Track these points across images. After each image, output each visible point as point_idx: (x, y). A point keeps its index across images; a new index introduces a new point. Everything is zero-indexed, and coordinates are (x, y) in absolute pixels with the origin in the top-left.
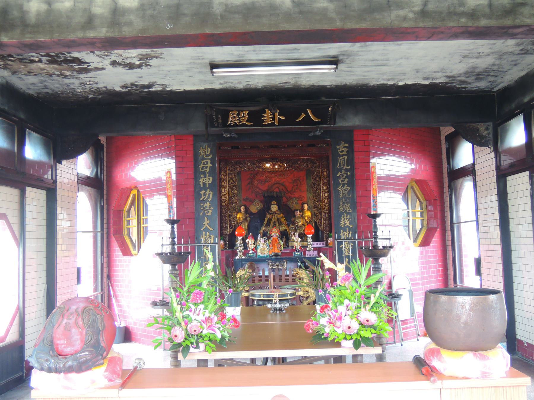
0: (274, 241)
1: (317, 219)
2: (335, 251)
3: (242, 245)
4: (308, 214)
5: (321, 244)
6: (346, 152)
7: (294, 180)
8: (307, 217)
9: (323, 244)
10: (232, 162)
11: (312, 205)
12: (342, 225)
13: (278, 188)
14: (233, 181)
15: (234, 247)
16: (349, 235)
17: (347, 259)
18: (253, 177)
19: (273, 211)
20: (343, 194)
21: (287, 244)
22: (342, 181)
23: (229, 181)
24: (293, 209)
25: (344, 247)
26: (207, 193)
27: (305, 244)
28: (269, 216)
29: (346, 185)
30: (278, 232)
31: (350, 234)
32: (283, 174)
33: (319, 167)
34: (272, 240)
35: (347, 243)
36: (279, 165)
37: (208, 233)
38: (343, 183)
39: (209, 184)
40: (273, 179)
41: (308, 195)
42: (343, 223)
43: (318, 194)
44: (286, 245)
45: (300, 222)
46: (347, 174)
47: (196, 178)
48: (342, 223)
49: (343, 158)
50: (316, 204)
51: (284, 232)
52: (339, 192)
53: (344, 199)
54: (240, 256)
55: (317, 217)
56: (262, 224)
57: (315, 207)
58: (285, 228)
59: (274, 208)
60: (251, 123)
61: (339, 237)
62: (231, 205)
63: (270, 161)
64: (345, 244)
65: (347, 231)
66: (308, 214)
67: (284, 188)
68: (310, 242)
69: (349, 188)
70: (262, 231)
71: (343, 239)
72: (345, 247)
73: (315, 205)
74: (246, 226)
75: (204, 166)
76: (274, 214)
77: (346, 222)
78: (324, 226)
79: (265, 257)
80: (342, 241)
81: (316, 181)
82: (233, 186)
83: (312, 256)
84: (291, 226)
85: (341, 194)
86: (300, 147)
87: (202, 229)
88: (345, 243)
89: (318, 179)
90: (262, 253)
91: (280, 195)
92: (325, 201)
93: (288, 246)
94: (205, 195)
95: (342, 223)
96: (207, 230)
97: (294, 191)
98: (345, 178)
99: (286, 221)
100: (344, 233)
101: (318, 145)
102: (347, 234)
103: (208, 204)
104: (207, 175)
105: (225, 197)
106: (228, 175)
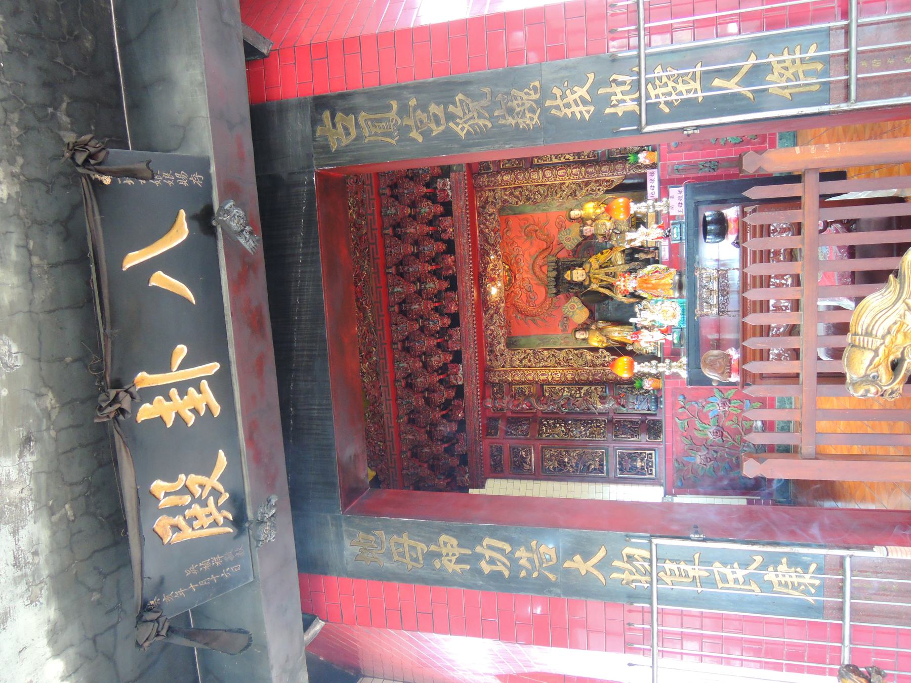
0: (645, 286)
1: (599, 190)
2: (683, 129)
4: (590, 208)
5: (653, 178)
6: (347, 115)
7: (525, 237)
8: (597, 208)
9: (652, 174)
10: (490, 360)
11: (571, 202)
12: (588, 112)
16: (624, 83)
17: (717, 82)
18: (522, 313)
20: (480, 116)
22: (438, 123)
23: (525, 366)
24: (581, 239)
25: (668, 99)
26: (488, 554)
28: (594, 286)
29: (451, 108)
30: (625, 278)
31: (621, 78)
33: (494, 190)
35: (655, 88)
37: (616, 563)
38: (443, 121)
39: (459, 545)
40: (525, 276)
41: (555, 207)
42: (581, 108)
43: (548, 191)
45: (604, 224)
46: (415, 108)
47: (443, 580)
48: (581, 112)
49: (367, 125)
50: (569, 194)
51: (627, 255)
52: (475, 131)
53: (496, 114)
54: (680, 367)
56: (612, 299)
57: (573, 194)
58: (619, 254)
59: (578, 275)
60: (216, 456)
61: (633, 118)
62: (572, 361)
63: (485, 289)
64: (657, 96)
65: (609, 90)
67: (542, 256)
69: (460, 97)
71: (640, 105)
72: (670, 94)
73: (571, 195)
74: (615, 328)
75: (407, 555)
77: (576, 96)
78: (613, 175)
80: (647, 105)
83: (683, 201)
84: (614, 243)
85: (481, 122)
86: (453, 231)
87: (603, 581)
88: (653, 93)
90: (674, 316)
91: (554, 264)
92: (560, 176)
94: (492, 561)
95: (581, 112)
96: (604, 565)
97: (547, 236)
98: (427, 111)
100: (614, 102)
101: (448, 195)
102: (618, 90)
103: (521, 553)
104: (433, 548)
105: (556, 374)
106: (514, 367)
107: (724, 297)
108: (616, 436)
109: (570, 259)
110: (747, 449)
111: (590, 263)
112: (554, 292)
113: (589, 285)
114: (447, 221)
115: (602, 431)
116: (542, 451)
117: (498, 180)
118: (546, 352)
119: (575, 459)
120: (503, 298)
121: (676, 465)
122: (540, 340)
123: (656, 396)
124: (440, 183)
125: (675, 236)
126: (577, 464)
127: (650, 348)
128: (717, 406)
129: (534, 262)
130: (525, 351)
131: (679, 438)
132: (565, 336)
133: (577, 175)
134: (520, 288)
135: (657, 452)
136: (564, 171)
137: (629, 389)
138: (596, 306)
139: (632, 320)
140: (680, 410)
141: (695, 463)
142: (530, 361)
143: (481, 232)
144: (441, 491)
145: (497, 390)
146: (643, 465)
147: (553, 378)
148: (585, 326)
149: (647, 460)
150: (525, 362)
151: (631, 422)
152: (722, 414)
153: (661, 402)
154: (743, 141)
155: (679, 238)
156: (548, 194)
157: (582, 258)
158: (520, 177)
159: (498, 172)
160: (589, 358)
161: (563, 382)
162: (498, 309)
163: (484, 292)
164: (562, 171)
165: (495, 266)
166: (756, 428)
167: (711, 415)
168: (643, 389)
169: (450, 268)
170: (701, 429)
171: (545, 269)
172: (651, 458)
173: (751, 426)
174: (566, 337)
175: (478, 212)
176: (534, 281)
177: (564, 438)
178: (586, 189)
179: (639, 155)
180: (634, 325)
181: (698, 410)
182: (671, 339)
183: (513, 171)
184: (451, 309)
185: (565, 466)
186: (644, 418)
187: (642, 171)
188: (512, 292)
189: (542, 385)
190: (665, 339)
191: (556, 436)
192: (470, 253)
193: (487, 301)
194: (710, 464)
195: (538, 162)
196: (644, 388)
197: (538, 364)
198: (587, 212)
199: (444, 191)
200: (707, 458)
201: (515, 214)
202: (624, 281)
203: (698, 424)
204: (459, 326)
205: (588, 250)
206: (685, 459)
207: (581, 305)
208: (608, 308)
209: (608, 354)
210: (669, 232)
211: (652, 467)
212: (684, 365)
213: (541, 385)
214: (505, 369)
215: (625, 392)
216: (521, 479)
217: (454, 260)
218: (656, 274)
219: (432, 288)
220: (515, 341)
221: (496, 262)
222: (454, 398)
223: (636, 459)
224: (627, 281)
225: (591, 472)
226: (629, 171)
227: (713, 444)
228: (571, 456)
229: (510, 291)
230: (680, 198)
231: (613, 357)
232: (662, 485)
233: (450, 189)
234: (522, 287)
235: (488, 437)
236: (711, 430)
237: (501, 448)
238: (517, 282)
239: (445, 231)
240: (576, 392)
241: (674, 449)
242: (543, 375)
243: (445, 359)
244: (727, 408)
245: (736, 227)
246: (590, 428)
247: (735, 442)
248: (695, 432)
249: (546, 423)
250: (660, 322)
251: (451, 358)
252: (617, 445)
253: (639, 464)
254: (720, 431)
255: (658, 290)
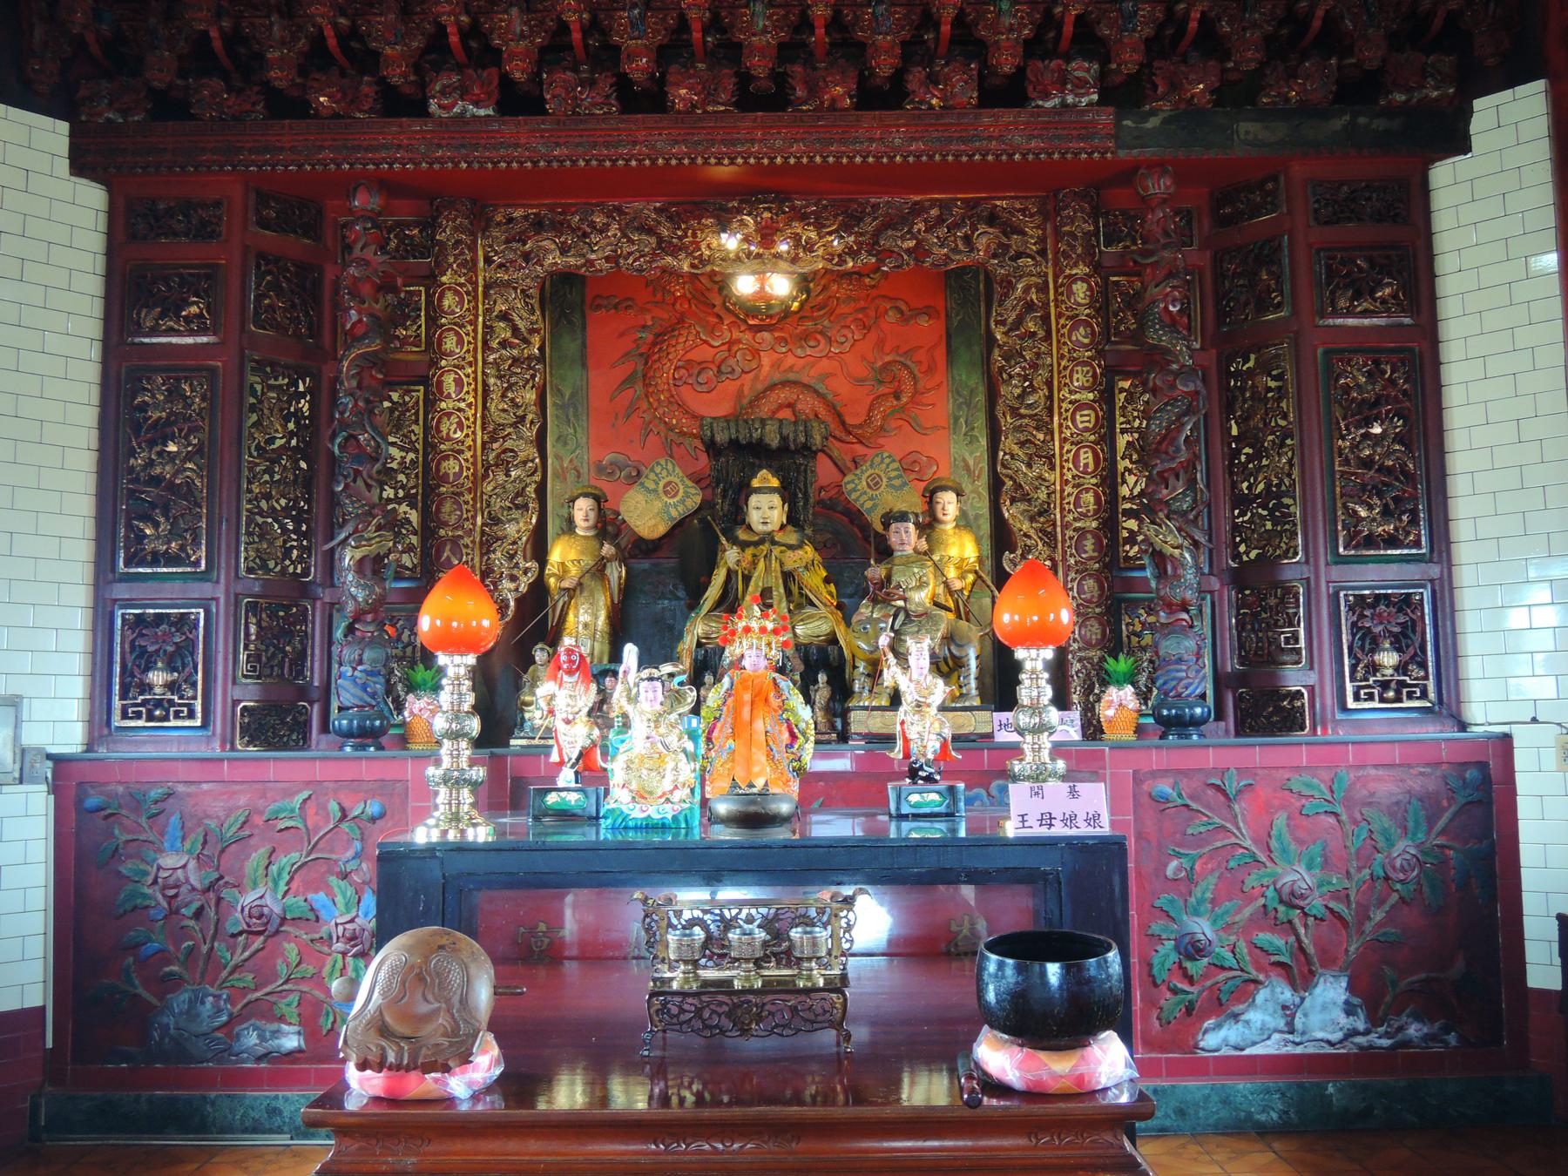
0: (747, 697)
3: (474, 725)
8: (958, 568)
10: (511, 220)
13: (790, 405)
14: (515, 331)
15: (510, 735)
18: (654, 344)
27: (1002, 727)
28: (731, 555)
30: (776, 632)
33: (1043, 252)
34: (728, 693)
36: (796, 238)
43: (1031, 417)
44: (833, 727)
45: (922, 585)
50: (1021, 480)
51: (822, 650)
54: (455, 818)
55: (1023, 556)
56: (694, 604)
62: (501, 478)
66: (962, 546)
76: (765, 548)
81: (1021, 337)
82: (516, 361)
83: (1059, 830)
86: (931, 107)
89: (1031, 326)
90: (640, 796)
93: (844, 737)
99: (832, 588)
101: (1046, 96)
105: (460, 426)
106: (486, 295)
107: (729, 1015)
108: (253, 608)
110: (208, 1006)
111: (800, 546)
112: (718, 438)
113: (734, 541)
114: (963, 87)
115: (271, 564)
116: (198, 369)
117: (1076, 265)
118: (531, 396)
119: (175, 475)
120: (708, 268)
121: (154, 793)
123: (384, 733)
124: (1082, 69)
125: (915, 798)
126: (156, 481)
127: (538, 714)
128: (348, 917)
129: (807, 387)
130: (537, 330)
131: (243, 800)
132: (584, 471)
133: (1077, 504)
134: (731, 343)
135: (200, 733)
136: (1091, 468)
137: (409, 650)
138: (671, 563)
139: (630, 652)
140: (333, 806)
141: (160, 851)
142: (504, 344)
143: (918, 210)
144: (845, 1000)
145: (411, 237)
146: (158, 690)
147: (449, 415)
148: (610, 528)
149: (172, 703)
150: (503, 331)
151: (301, 656)
152: (323, 932)
153: (363, 747)
154: (1155, 985)
155: (905, 810)
156: (1023, 416)
157: (812, 524)
158: (1081, 335)
159: (1097, 268)
160: (511, 529)
161: (434, 446)
162: (674, 251)
163: (728, 210)
165: (809, 247)
166: (276, 1034)
167: (319, 898)
168: (407, 693)
169: (814, 91)
170: (274, 868)
171: (786, 414)
172: (177, 715)
173: (282, 1019)
175: (978, 202)
176: (749, 386)
177: (246, 443)
178: (1032, 533)
179: (1129, 689)
180: (613, 667)
181: (336, 861)
182: (561, 783)
183: (1098, 311)
184: (678, 85)
185: (152, 443)
186: (315, 695)
187: (1075, 698)
188: (719, 317)
189: (424, 380)
191: (254, 417)
192: (858, 159)
193: (699, 218)
194: (160, 897)
195: (1122, 390)
196: (411, 697)
197: (493, 372)
198: (952, 540)
199: (1062, 82)
200: (177, 886)
201: (949, 337)
202: (763, 630)
203: (286, 860)
204: (622, 111)
205: (834, 545)
206: (175, 820)
207: (676, 513)
208: (663, 597)
209: (523, 588)
211: (150, 718)
212: (463, 832)
213: (425, 377)
214: (481, 263)
216: (108, 298)
217: (839, 105)
218: (786, 735)
219: (751, 23)
220: (570, 322)
221: (820, 252)
222: (382, 82)
223: (174, 669)
225: (129, 527)
226: (1080, 660)
227: (223, 904)
228: (184, 461)
229: (722, 313)
230: (1070, 820)
231: (512, 604)
232: (90, 747)
233: (1064, 105)
234: (735, 349)
235: (253, 196)
236: (268, 900)
237: (212, 235)
239: (933, 80)
240: (403, 487)
241: (205, 787)
242: (459, 383)
243: (513, 55)
244: (339, 946)
245: (1055, 1087)
246: (283, 527)
247: (231, 973)
248: (263, 851)
249: (301, 389)
250: (623, 747)
251: (517, 75)
252: (221, 609)
253: (158, 678)
254: (267, 927)
255: (731, 741)
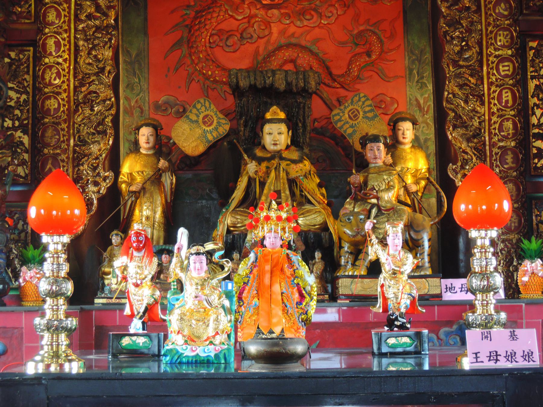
0: (268, 268)
7: (356, 32)
8: (414, 176)
13: (293, 61)
18: (195, 18)
19: (271, 148)
21: (330, 289)
28: (251, 167)
32: (315, 10)
34: (254, 265)
40: (275, 29)
43: (467, 67)
44: (326, 291)
45: (389, 188)
50: (461, 113)
51: (317, 235)
54: (56, 355)
55: (462, 167)
56: (224, 201)
62: (88, 112)
66: (417, 161)
68: (484, 275)
70: (221, 230)
74: (159, 215)
76: (275, 162)
79: (207, 362)
82: (98, 29)
83: (503, 364)
90: (190, 340)
92: (500, 94)
97: (358, 77)
99: (324, 191)
105: (58, 75)
109: (309, 121)
111: (301, 161)
112: (241, 84)
113: (253, 157)
118: (108, 53)
122: (137, 55)
129: (304, 48)
130: (113, 7)
133: (501, 129)
134: (250, 17)
142: (90, 17)
147: (51, 67)
148: (164, 149)
155: (385, 350)
156: (461, 67)
157: (309, 145)
160: (94, 148)
161: (40, 90)
164: (510, 98)
168: (21, 266)
174: (142, 111)
189: (34, 43)
190: (132, 316)
195: (531, 48)
196: (24, 268)
201: (405, 12)
208: (202, 198)
209: (103, 191)
210: (402, 327)
215: (16, 227)
218: (296, 296)
224: (280, 225)
230: (511, 356)
231: (95, 202)
238: (262, 12)
240: (18, 119)
242: (58, 45)
255: (256, 300)
